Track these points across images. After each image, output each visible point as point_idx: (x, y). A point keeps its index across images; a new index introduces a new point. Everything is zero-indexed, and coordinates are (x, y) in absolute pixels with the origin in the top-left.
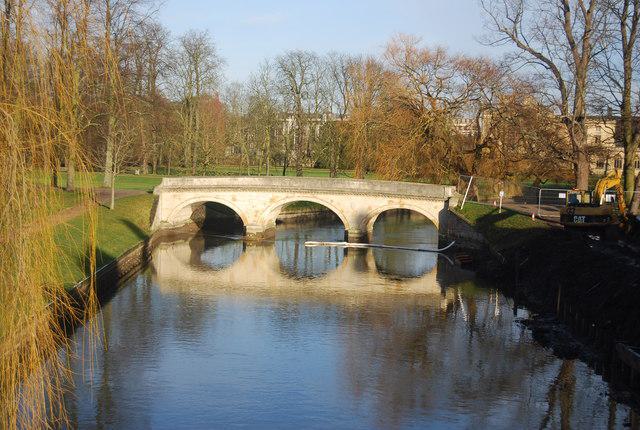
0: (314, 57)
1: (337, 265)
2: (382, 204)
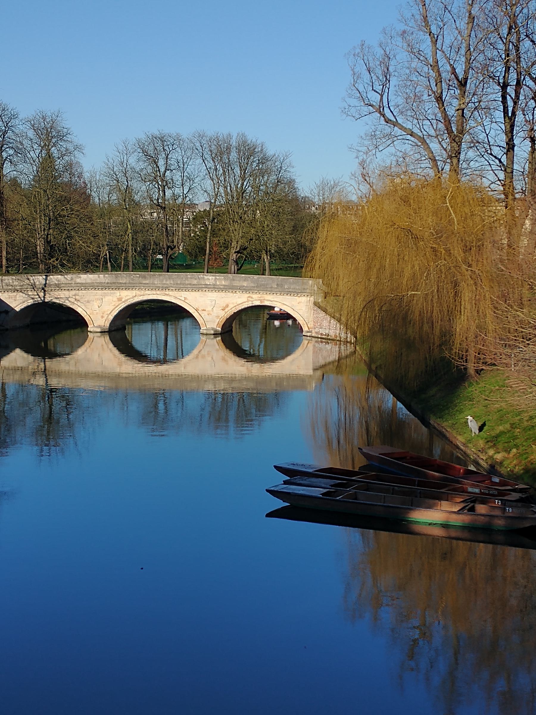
0: (178, 138)
1: (183, 357)
2: (240, 301)
